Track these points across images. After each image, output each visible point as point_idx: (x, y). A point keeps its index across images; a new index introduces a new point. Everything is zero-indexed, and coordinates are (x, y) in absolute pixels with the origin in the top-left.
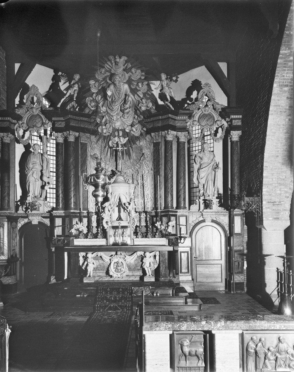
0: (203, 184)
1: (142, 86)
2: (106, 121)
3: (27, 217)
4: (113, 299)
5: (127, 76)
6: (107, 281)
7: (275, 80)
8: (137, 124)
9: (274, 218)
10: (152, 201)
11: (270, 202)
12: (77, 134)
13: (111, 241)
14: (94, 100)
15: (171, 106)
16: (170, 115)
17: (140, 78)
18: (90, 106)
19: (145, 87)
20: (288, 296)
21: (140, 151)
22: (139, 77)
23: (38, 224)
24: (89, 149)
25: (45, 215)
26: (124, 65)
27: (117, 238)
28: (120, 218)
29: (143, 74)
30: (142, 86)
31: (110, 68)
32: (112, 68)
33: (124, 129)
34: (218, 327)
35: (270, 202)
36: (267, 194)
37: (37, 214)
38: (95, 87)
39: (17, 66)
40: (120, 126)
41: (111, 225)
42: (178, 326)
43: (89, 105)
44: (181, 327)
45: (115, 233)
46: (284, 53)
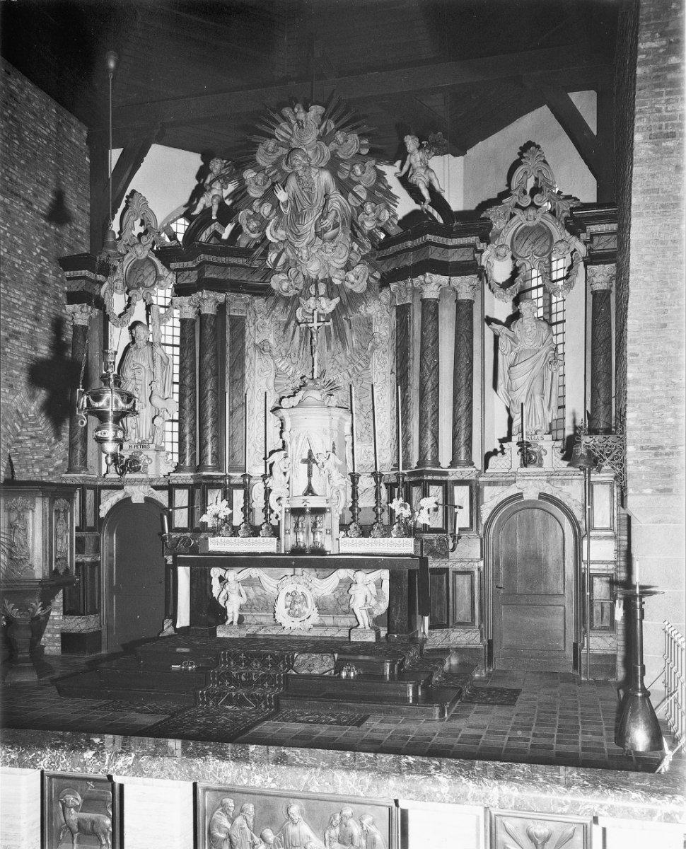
0: (522, 404)
1: (363, 173)
2: (287, 261)
3: (120, 488)
4: (243, 678)
5: (327, 151)
6: (276, 635)
7: (637, 124)
8: (358, 264)
9: (657, 490)
10: (392, 447)
11: (648, 448)
12: (221, 297)
13: (289, 541)
14: (256, 216)
15: (436, 214)
16: (429, 237)
17: (359, 154)
18: (247, 230)
19: (371, 174)
20: (642, 697)
21: (366, 329)
22: (354, 151)
23: (143, 502)
24: (249, 330)
25: (159, 484)
26: (319, 127)
27: (301, 537)
28: (309, 491)
29: (365, 142)
30: (363, 173)
31: (288, 137)
32: (292, 136)
34: (118, 767)
35: (648, 448)
36: (639, 426)
37: (141, 481)
38: (256, 184)
39: (115, 155)
40: (319, 271)
41: (289, 506)
42: (31, 757)
43: (244, 228)
44: (38, 760)
45: (297, 524)
46: (650, 48)
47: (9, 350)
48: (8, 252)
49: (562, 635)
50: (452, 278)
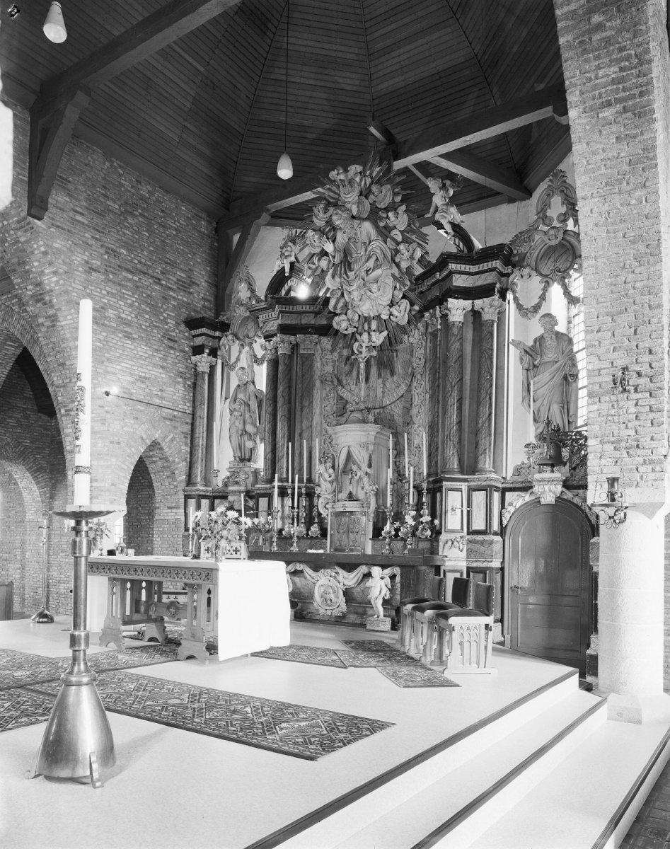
31: (336, 196)
33: (379, 316)
47: (135, 391)
48: (136, 317)
49: (44, 600)
50: (475, 301)
